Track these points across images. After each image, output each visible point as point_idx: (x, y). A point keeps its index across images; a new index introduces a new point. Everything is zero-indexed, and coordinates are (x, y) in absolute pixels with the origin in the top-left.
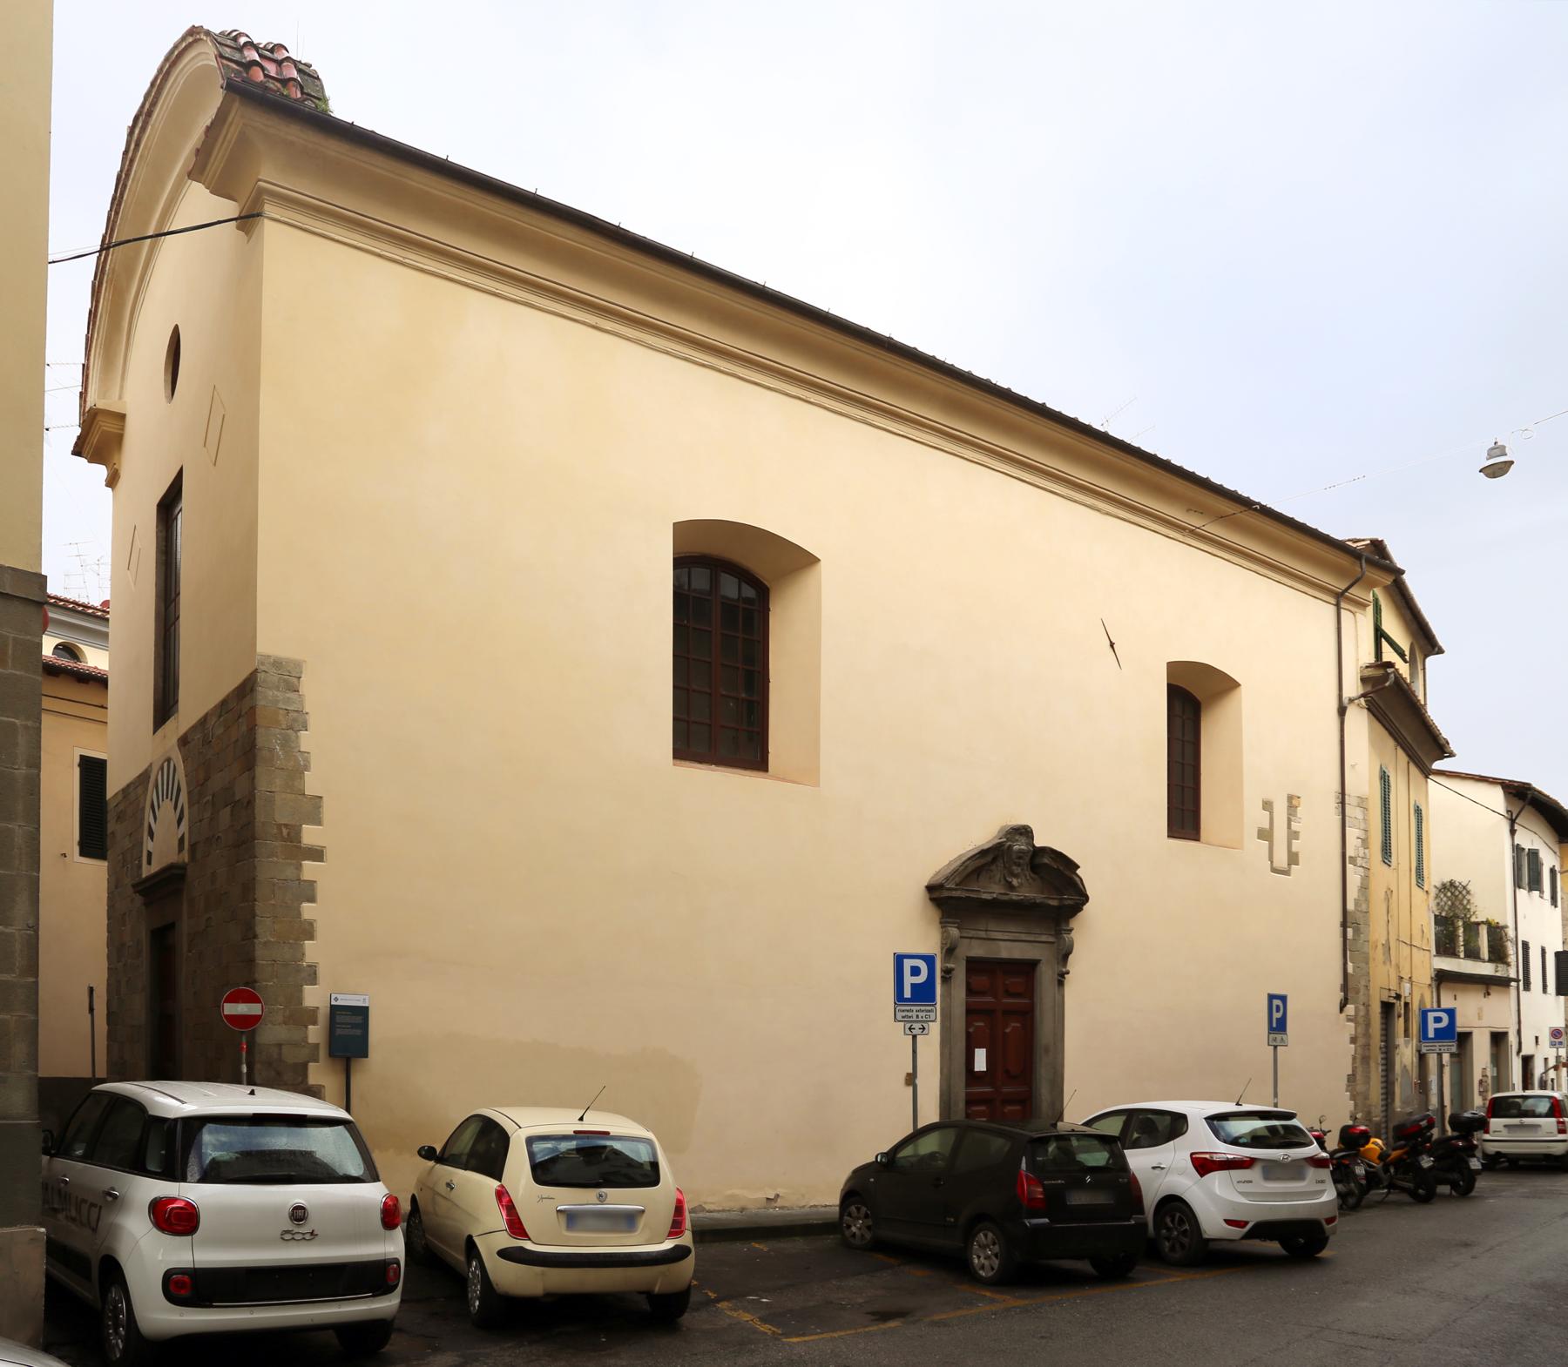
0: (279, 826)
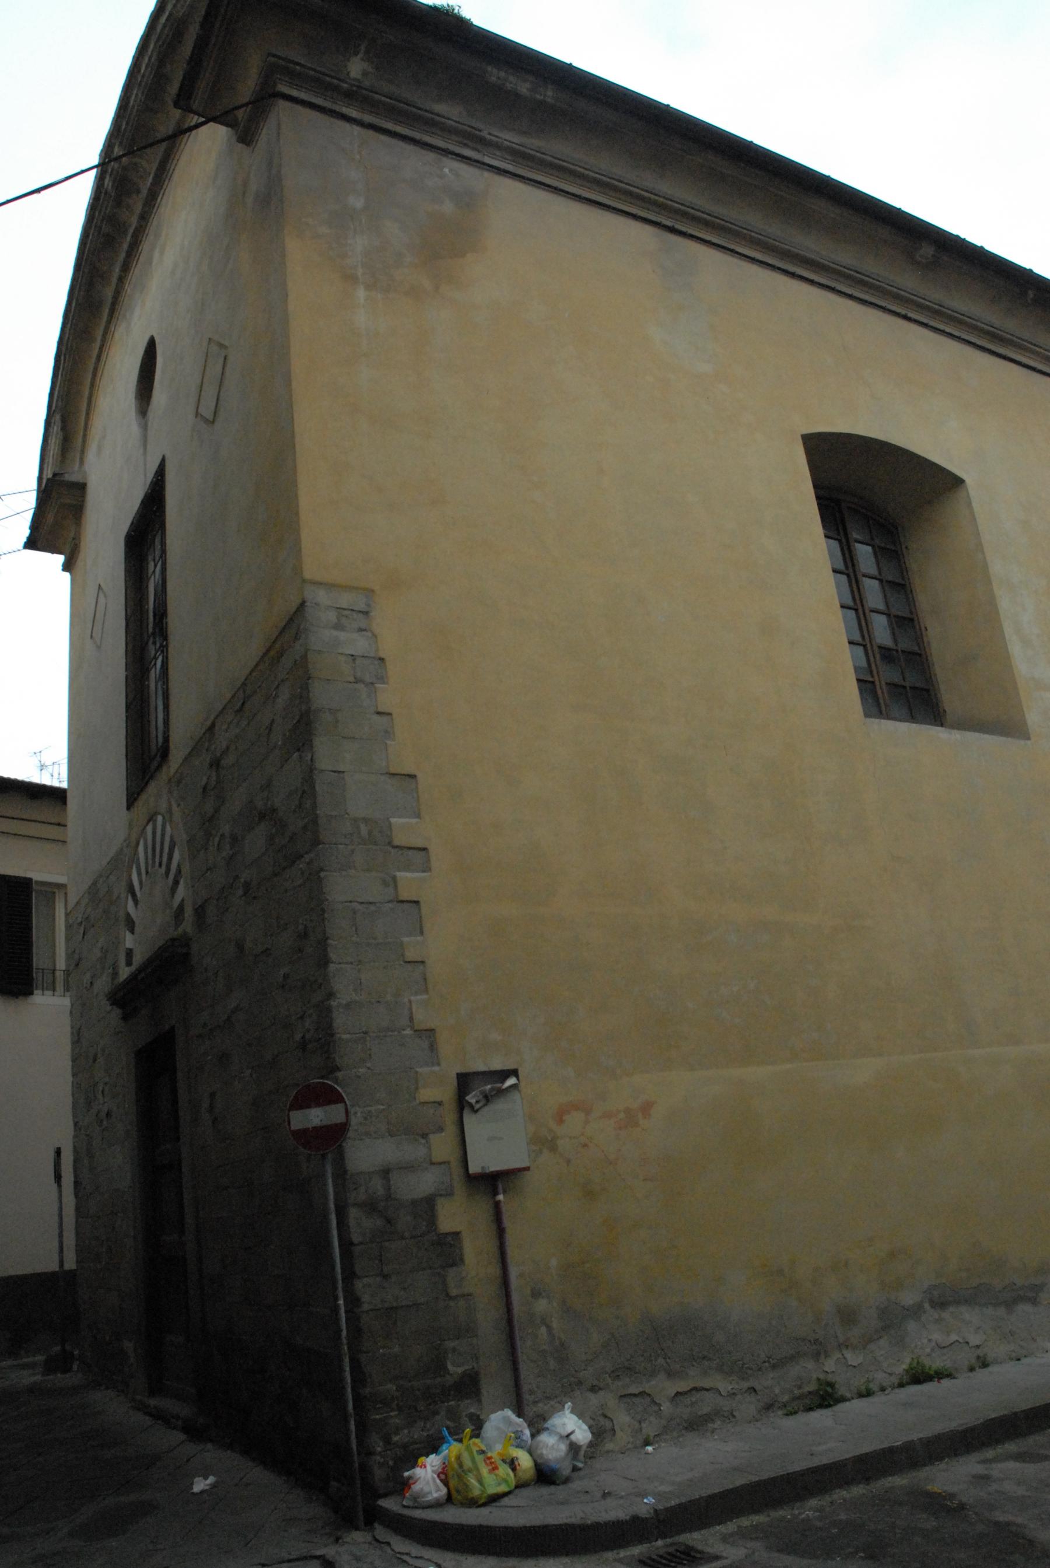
0: (356, 820)
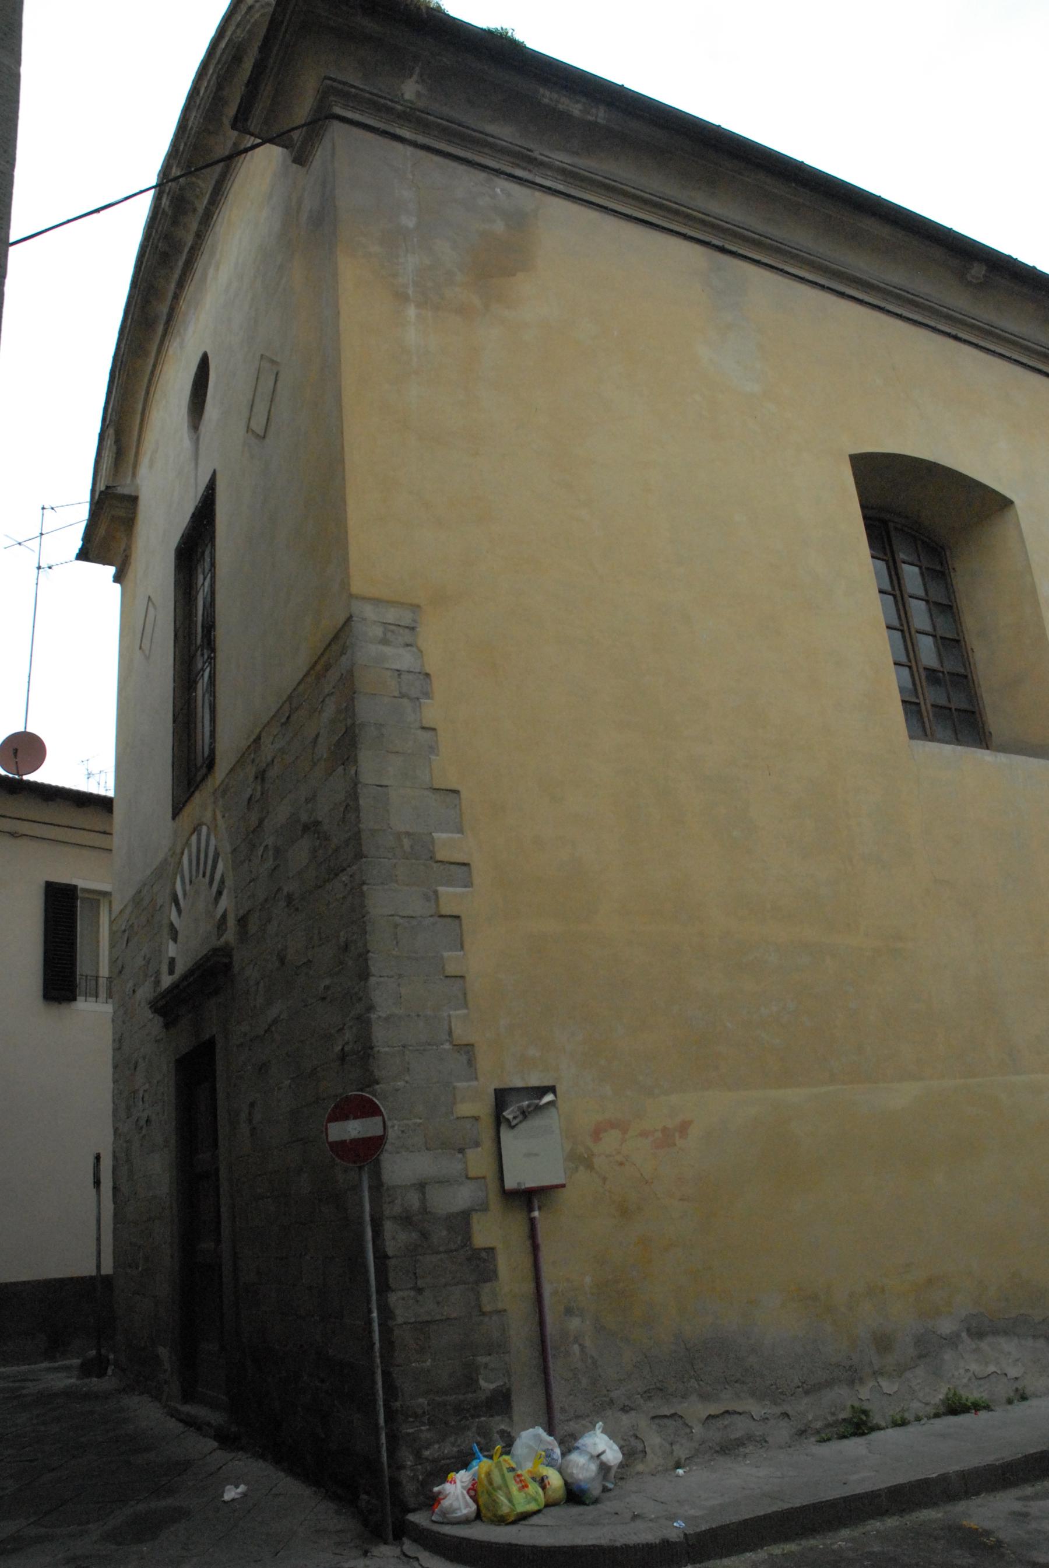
0: (398, 836)
